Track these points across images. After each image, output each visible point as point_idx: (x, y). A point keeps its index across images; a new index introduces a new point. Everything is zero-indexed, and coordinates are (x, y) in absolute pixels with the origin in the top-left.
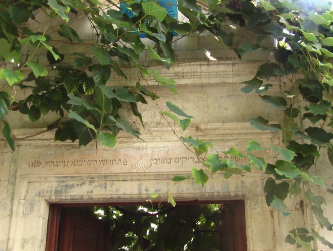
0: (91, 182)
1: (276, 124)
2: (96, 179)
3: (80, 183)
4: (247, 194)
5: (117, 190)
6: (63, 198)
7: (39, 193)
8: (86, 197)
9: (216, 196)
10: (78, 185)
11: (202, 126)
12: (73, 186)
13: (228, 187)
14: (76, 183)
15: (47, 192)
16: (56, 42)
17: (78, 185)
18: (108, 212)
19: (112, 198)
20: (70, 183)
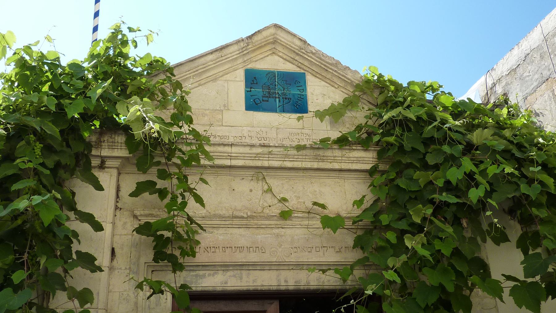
5: (254, 281)
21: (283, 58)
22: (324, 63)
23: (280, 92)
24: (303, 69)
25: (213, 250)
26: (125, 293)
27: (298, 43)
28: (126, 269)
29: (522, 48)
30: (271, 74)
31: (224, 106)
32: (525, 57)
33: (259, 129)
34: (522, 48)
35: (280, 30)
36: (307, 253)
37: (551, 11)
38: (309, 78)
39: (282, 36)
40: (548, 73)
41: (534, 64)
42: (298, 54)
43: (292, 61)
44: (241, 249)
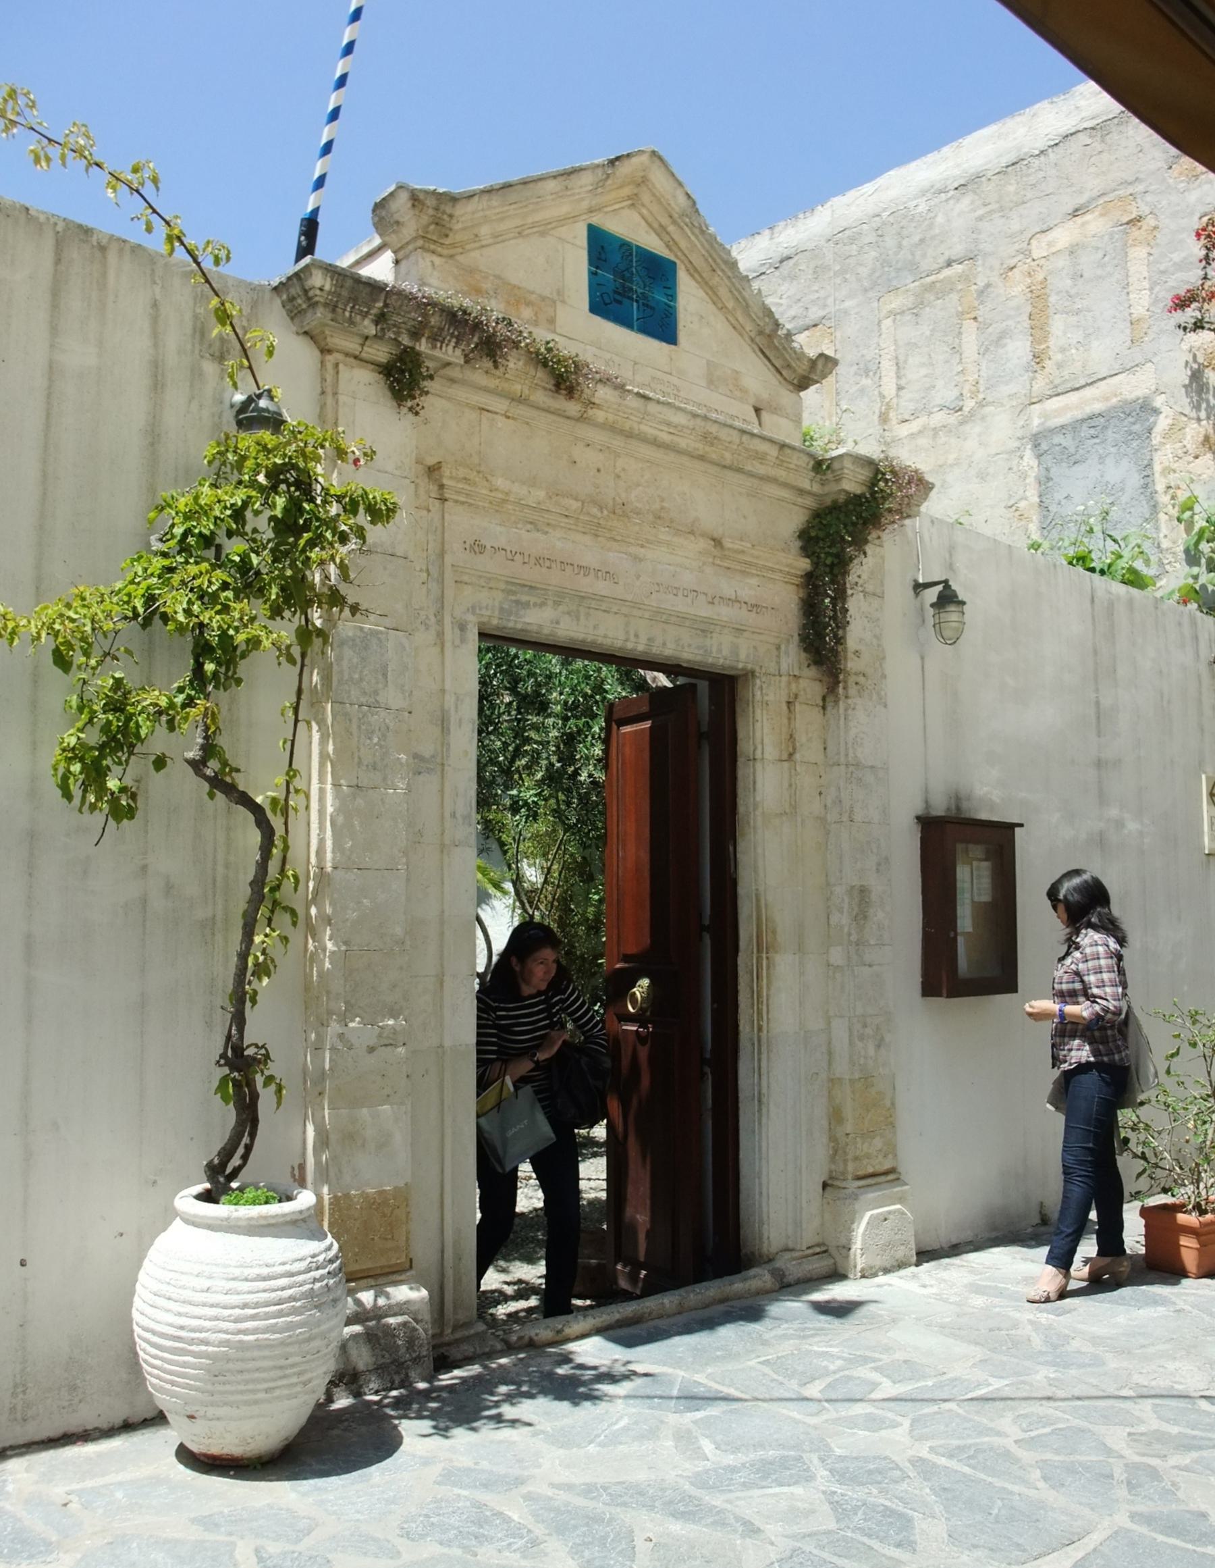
0: (557, 603)
1: (960, 962)
2: (567, 600)
3: (539, 601)
4: (757, 669)
5: (595, 627)
6: (511, 625)
7: (473, 608)
8: (546, 631)
9: (1110, 961)
10: (535, 605)
11: (727, 543)
12: (526, 605)
13: (737, 655)
14: (533, 600)
15: (487, 608)
16: (685, 460)
17: (535, 605)
18: (288, 544)
19: (583, 641)
20: (524, 598)
21: (646, 221)
22: (715, 256)
23: (640, 291)
24: (676, 256)
25: (548, 563)
26: (422, 613)
27: (682, 199)
28: (421, 570)
29: (781, 239)
30: (625, 247)
31: (559, 292)
32: (781, 262)
33: (608, 356)
34: (781, 239)
35: (658, 162)
36: (671, 596)
37: (862, 184)
38: (683, 277)
39: (658, 178)
40: (822, 313)
41: (795, 282)
42: (674, 222)
43: (661, 231)
44: (584, 570)
